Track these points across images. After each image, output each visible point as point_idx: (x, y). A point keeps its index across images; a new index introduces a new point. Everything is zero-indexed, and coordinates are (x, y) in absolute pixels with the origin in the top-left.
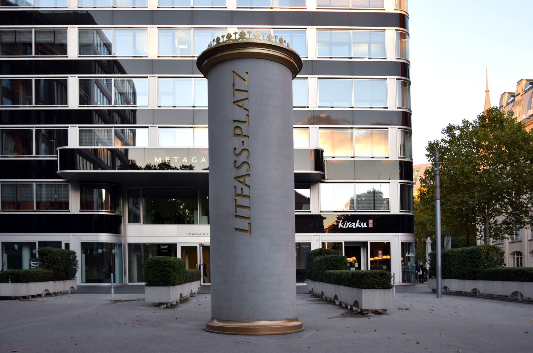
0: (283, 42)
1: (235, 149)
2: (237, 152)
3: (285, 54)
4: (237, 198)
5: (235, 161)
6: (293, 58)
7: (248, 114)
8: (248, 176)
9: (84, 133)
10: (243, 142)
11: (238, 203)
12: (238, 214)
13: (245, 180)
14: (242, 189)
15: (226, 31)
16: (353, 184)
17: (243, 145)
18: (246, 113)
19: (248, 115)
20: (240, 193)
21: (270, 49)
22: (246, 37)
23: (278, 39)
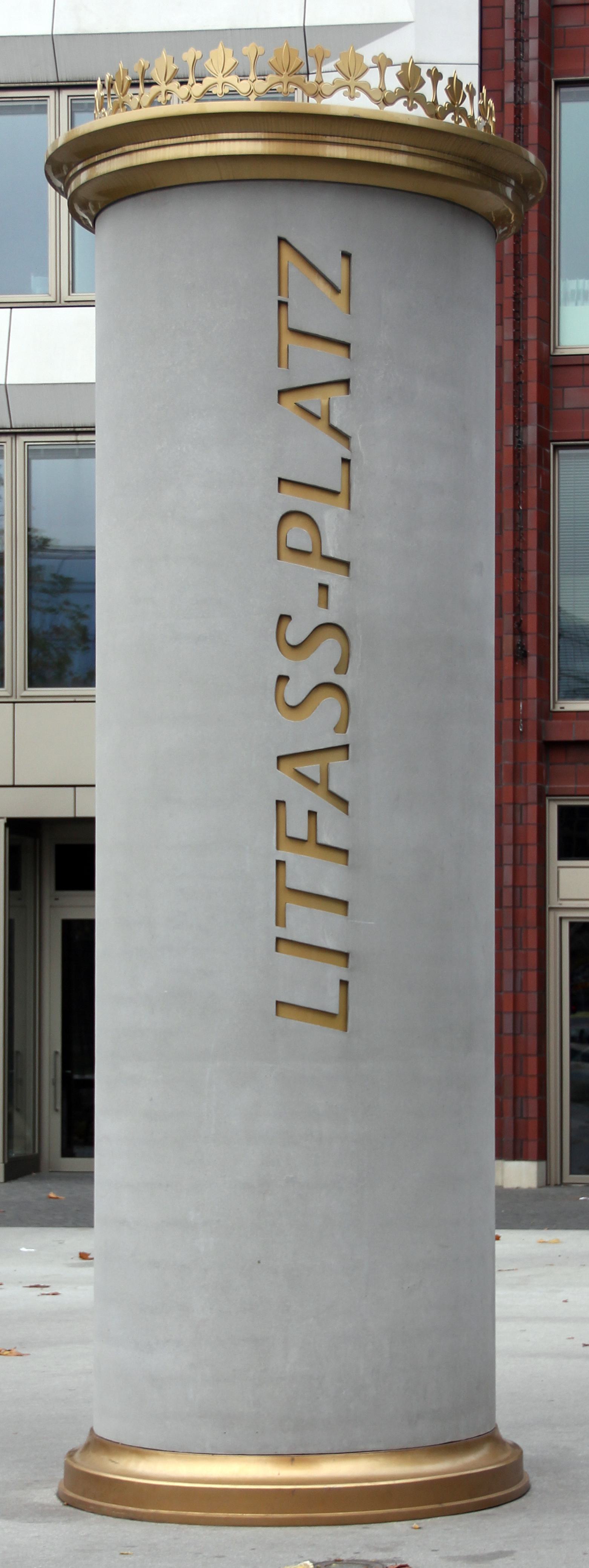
0: (423, 82)
1: (284, 618)
2: (295, 633)
3: (284, 136)
4: (288, 855)
5: (282, 679)
6: (403, 148)
7: (347, 456)
8: (342, 753)
9: (280, 1005)
10: (323, 587)
11: (292, 882)
12: (334, 972)
13: (326, 775)
14: (312, 814)
15: (43, 109)
16: (19, 421)
17: (324, 602)
18: (342, 451)
19: (346, 461)
20: (302, 833)
21: (210, 133)
22: (463, 107)
23: (443, 84)
